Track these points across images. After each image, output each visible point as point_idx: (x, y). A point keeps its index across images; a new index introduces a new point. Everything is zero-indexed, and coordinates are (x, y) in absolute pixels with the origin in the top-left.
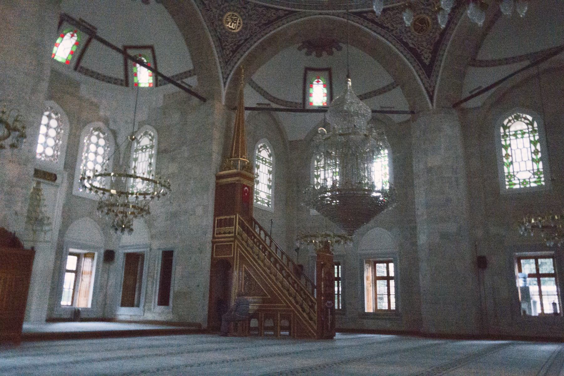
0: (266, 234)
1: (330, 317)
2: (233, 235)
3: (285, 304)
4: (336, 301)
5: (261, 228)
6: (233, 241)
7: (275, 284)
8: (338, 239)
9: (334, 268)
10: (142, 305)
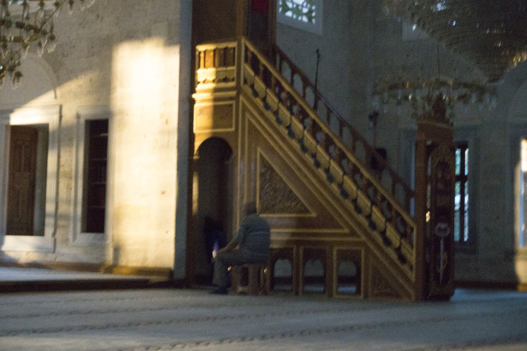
0: (306, 82)
1: (443, 256)
2: (232, 84)
3: (346, 231)
4: (457, 224)
5: (294, 70)
6: (236, 98)
7: (342, 206)
8: (463, 91)
9: (454, 155)
10: (49, 231)
